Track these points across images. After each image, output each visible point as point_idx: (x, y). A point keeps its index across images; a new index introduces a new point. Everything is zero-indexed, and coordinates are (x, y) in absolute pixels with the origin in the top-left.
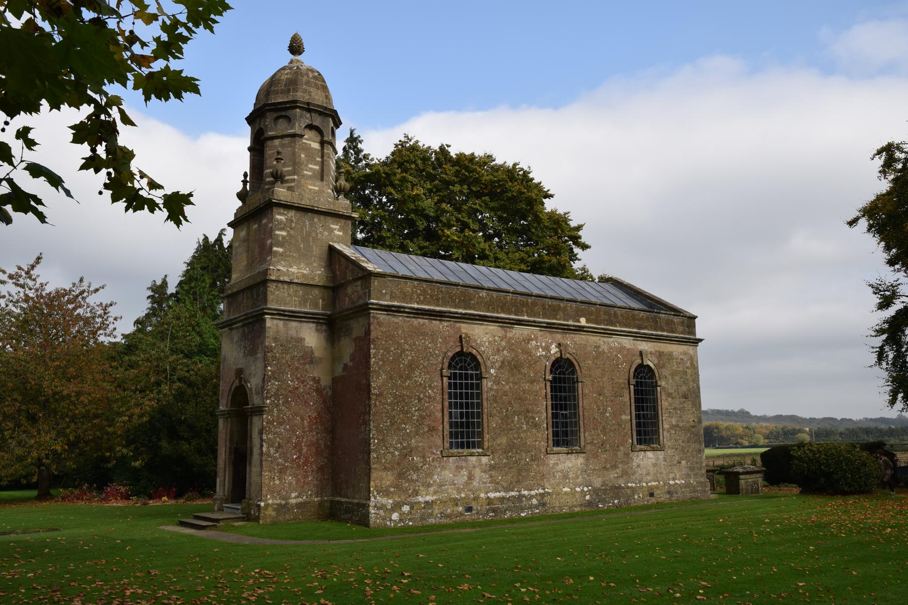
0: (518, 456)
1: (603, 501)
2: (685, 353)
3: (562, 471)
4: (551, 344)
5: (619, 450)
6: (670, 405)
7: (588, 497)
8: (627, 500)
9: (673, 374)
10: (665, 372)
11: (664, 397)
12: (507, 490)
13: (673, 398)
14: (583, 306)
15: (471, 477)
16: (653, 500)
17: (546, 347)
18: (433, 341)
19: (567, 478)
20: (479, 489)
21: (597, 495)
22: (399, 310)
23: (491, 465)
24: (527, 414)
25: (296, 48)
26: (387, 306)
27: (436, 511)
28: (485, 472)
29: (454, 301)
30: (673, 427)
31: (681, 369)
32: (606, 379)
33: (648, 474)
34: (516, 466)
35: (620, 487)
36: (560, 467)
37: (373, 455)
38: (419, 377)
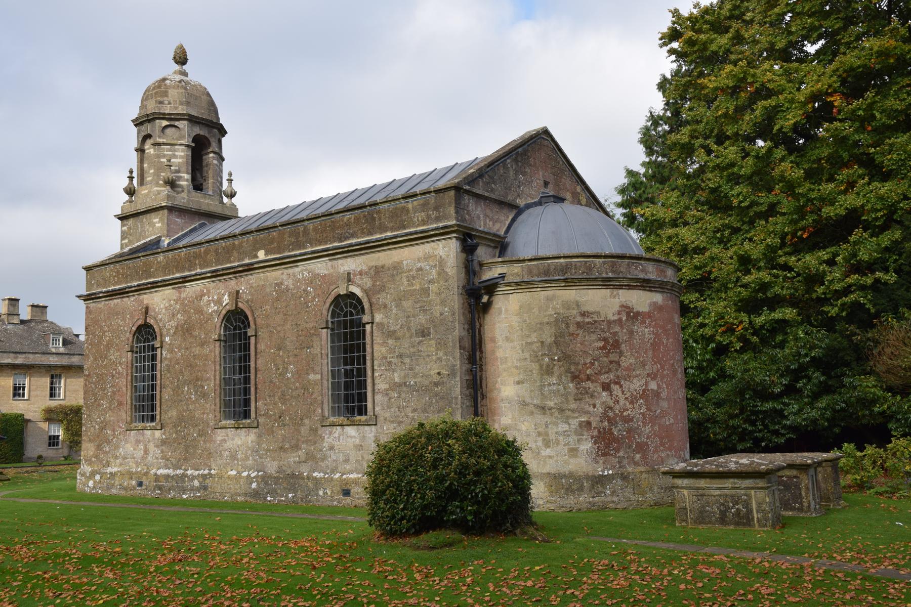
0: (186, 431)
1: (273, 493)
2: (427, 258)
3: (229, 450)
4: (224, 295)
5: (303, 425)
6: (391, 350)
7: (254, 485)
8: (307, 496)
9: (399, 300)
10: (382, 298)
11: (378, 339)
12: (176, 467)
13: (397, 339)
14: (262, 235)
15: (146, 452)
16: (348, 500)
17: (215, 298)
18: (124, 319)
19: (236, 457)
20: (152, 465)
21: (266, 483)
22: (112, 294)
23: (162, 440)
24: (196, 382)
25: (181, 59)
26: (120, 290)
27: (117, 483)
28: (157, 446)
29: (138, 274)
30: (394, 386)
31: (417, 287)
32: (288, 326)
33: (347, 460)
34: (186, 445)
35: (300, 477)
36: (228, 445)
37: (84, 428)
38: (113, 355)
